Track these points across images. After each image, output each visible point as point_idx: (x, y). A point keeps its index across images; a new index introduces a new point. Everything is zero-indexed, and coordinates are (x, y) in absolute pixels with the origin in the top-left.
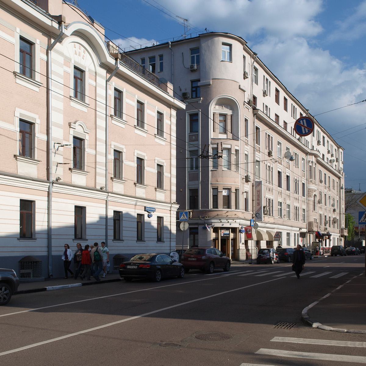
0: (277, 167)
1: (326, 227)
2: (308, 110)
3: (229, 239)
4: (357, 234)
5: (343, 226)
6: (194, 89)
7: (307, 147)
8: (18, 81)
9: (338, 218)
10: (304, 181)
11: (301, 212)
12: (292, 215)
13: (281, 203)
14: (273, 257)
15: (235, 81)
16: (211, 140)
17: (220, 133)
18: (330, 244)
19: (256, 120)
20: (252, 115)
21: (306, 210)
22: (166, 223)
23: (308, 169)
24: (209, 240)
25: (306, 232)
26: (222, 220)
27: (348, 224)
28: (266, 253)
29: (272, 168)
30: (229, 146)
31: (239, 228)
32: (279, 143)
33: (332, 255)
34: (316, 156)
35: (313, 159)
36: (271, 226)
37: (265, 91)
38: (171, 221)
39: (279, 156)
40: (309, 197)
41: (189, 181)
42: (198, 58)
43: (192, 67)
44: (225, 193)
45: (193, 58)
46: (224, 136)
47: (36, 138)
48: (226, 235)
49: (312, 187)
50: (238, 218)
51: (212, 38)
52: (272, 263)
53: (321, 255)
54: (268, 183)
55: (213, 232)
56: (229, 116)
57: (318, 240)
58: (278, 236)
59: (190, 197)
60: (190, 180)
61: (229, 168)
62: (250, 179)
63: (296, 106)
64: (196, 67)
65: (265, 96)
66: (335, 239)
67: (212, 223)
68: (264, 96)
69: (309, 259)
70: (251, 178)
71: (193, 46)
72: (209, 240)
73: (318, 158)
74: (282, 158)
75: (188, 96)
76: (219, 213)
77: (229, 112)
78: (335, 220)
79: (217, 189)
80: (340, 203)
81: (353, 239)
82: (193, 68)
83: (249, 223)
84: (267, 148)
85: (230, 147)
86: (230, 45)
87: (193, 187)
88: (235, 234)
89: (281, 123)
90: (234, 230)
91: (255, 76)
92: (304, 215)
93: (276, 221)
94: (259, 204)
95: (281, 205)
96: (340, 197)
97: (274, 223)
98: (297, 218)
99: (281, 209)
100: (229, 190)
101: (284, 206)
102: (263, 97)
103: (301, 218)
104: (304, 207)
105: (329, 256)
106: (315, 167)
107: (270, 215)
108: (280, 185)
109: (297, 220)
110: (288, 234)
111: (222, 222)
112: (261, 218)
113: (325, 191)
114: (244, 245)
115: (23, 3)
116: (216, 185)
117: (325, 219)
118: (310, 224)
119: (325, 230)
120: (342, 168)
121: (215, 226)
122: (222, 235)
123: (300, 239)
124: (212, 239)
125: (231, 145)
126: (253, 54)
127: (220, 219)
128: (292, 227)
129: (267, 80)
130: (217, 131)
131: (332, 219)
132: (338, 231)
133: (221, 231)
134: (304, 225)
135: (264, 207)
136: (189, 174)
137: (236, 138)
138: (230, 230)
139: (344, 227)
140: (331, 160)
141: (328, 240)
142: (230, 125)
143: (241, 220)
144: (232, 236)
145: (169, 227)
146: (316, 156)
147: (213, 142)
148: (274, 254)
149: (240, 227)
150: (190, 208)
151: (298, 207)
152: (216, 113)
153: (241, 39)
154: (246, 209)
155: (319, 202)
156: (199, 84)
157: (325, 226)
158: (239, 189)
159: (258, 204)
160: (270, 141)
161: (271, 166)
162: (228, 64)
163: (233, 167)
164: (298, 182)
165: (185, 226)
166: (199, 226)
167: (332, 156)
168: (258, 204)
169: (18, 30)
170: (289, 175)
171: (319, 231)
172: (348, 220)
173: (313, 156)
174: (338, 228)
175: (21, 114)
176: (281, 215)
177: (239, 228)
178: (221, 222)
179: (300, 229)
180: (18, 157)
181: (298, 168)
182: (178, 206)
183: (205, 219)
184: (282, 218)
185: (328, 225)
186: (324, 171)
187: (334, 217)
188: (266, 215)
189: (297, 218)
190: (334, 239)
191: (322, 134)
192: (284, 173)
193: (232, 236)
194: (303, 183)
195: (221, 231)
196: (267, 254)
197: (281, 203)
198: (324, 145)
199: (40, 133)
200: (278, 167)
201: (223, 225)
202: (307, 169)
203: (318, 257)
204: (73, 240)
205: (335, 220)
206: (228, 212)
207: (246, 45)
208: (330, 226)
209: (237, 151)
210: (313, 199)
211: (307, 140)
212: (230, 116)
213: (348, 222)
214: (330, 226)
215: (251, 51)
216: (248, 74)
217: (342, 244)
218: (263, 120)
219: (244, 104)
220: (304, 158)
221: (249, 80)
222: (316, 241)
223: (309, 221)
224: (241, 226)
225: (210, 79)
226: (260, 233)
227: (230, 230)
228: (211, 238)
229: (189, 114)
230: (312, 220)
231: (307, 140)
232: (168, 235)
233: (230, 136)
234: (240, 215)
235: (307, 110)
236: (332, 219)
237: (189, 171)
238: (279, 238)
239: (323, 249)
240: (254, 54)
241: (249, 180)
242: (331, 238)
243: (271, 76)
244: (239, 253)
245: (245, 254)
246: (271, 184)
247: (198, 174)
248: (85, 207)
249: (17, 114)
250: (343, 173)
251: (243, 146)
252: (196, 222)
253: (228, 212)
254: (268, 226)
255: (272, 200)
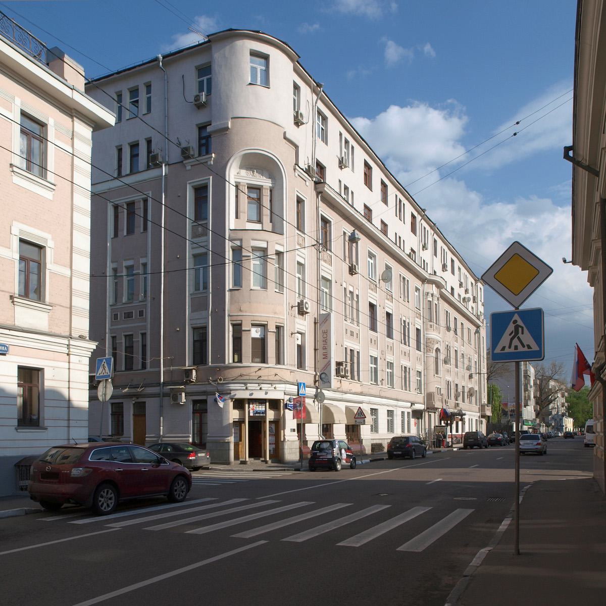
0: (368, 296)
1: (457, 402)
2: (425, 209)
3: (265, 422)
4: (505, 413)
5: (485, 400)
6: (204, 141)
7: (424, 269)
8: (16, 180)
9: (476, 388)
10: (419, 324)
11: (414, 378)
12: (397, 381)
13: (376, 359)
14: (339, 456)
15: (275, 124)
16: (229, 232)
17: (249, 221)
18: (456, 431)
19: (321, 204)
20: (314, 193)
21: (422, 373)
22: (52, 380)
23: (426, 306)
24: (225, 423)
25: (424, 410)
26: (249, 385)
27: (492, 398)
28: (326, 449)
29: (357, 296)
30: (264, 245)
31: (283, 400)
32: (371, 255)
33: (465, 447)
34: (439, 286)
35: (434, 289)
36: (358, 399)
37: (342, 158)
38: (71, 380)
39: (372, 277)
40: (427, 351)
41: (192, 312)
42: (209, 81)
43: (197, 98)
44: (256, 333)
45: (201, 84)
46: (258, 226)
47: (47, 272)
48: (259, 413)
49: (433, 335)
50: (280, 381)
51: (233, 42)
52: (336, 470)
53: (449, 447)
54: (349, 321)
55: (235, 408)
56: (265, 189)
57: (444, 423)
58: (362, 416)
59: (195, 341)
60: (193, 310)
61: (265, 287)
62: (307, 309)
63: (404, 201)
64: (204, 99)
65: (343, 167)
66: (473, 421)
67: (231, 390)
68: (341, 168)
69: (421, 456)
70: (311, 307)
71: (200, 60)
72: (225, 423)
73: (443, 290)
74: (377, 281)
75: (192, 153)
76: (243, 371)
77: (265, 183)
78: (471, 392)
79: (240, 325)
80: (480, 365)
81: (499, 421)
82: (199, 100)
83: (295, 389)
84: (347, 259)
85: (266, 247)
86: (266, 57)
87: (199, 323)
88: (277, 412)
89: (376, 222)
90: (275, 404)
91: (322, 129)
92: (420, 381)
93: (365, 391)
94: (327, 356)
95: (376, 363)
96: (479, 356)
97: (361, 394)
98: (408, 385)
99: (376, 369)
100: (264, 326)
101: (381, 365)
102: (295, 127)
103: (414, 385)
104: (420, 368)
105: (460, 448)
106: (437, 303)
107: (353, 378)
108: (373, 328)
109: (406, 390)
110: (390, 413)
111: (249, 388)
112: (329, 382)
113: (456, 345)
114: (296, 433)
115: (4, 43)
116: (239, 318)
117: (457, 390)
118: (430, 397)
119: (455, 406)
120: (483, 312)
121: (236, 397)
122: (251, 414)
123: (413, 421)
124: (231, 421)
125: (267, 242)
126: (315, 85)
127: (245, 384)
128: (397, 400)
129: (347, 142)
130: (244, 216)
131: (466, 390)
132: (476, 408)
133: (249, 407)
134: (420, 398)
135: (339, 364)
136: (192, 300)
137: (277, 230)
138: (267, 404)
139: (486, 403)
140: (464, 298)
141: (460, 423)
142: (265, 204)
143: (288, 386)
144: (270, 415)
145: (65, 392)
146: (439, 286)
147: (233, 235)
148: (343, 451)
149: (287, 398)
150: (194, 364)
151: (409, 368)
152: (241, 184)
153: (288, 48)
154: (301, 364)
155: (446, 362)
156: (209, 129)
157: (456, 400)
158: (283, 327)
159: (324, 357)
160: (406, 286)
161: (356, 292)
162: (261, 90)
163: (271, 285)
164: (409, 325)
165: (106, 391)
166: (208, 396)
167: (466, 291)
168: (324, 357)
169: (18, 101)
170: (391, 313)
171: (444, 407)
172: (492, 392)
173: (434, 285)
174: (476, 405)
175: (21, 231)
176: (376, 380)
177: (283, 400)
178: (246, 389)
179: (412, 404)
180: (15, 299)
181: (408, 302)
182: (93, 346)
183: (218, 384)
184: (393, 388)
185: (460, 398)
186: (453, 314)
187: (470, 386)
188: (345, 379)
189: (406, 385)
190: (470, 420)
191: (450, 256)
192: (382, 307)
193: (270, 415)
194: (417, 329)
195: (249, 407)
196: (327, 451)
197: (376, 359)
198: (453, 272)
199: (54, 263)
200: (369, 294)
201: (251, 394)
202: (423, 305)
203: (440, 451)
204: (16, 429)
205: (471, 392)
206: (260, 369)
207: (297, 62)
208: (463, 401)
209: (279, 254)
210: (434, 354)
211: (424, 261)
212: (267, 189)
213: (493, 396)
214: (463, 401)
215: (310, 78)
216: (304, 115)
217: (483, 430)
218: (336, 207)
219: (295, 169)
220: (388, 264)
221: (306, 129)
222: (441, 423)
223: (428, 392)
224: (289, 397)
225: (227, 119)
226: (330, 410)
227: (267, 404)
228: (229, 419)
229: (192, 186)
230: (432, 389)
231: (424, 261)
232: (63, 413)
233: (268, 225)
234: (287, 376)
235: (424, 211)
236: (466, 390)
237: (191, 292)
238: (363, 420)
239: (452, 437)
240: (318, 85)
241: (305, 310)
242: (466, 418)
243: (360, 143)
244: (283, 449)
245: (298, 450)
246: (355, 323)
247: (207, 298)
248: (43, 369)
249: (15, 231)
250: (483, 320)
251: (294, 245)
252: (202, 388)
253: (260, 369)
254: (342, 398)
255: (358, 353)
